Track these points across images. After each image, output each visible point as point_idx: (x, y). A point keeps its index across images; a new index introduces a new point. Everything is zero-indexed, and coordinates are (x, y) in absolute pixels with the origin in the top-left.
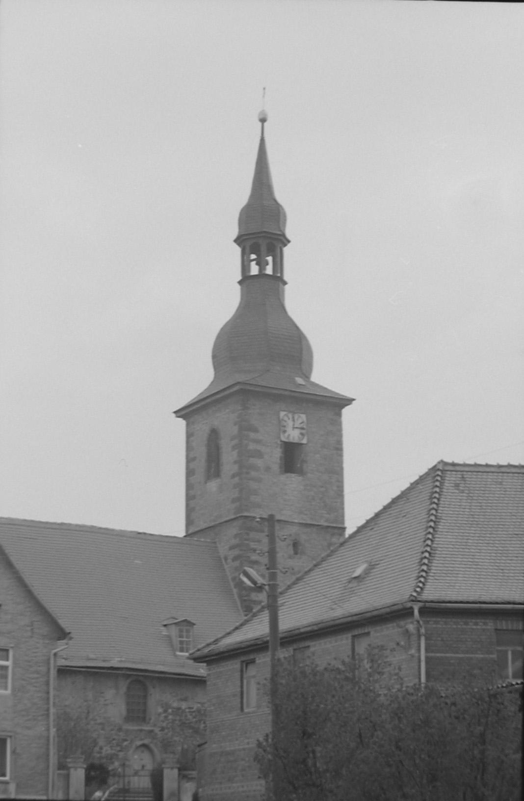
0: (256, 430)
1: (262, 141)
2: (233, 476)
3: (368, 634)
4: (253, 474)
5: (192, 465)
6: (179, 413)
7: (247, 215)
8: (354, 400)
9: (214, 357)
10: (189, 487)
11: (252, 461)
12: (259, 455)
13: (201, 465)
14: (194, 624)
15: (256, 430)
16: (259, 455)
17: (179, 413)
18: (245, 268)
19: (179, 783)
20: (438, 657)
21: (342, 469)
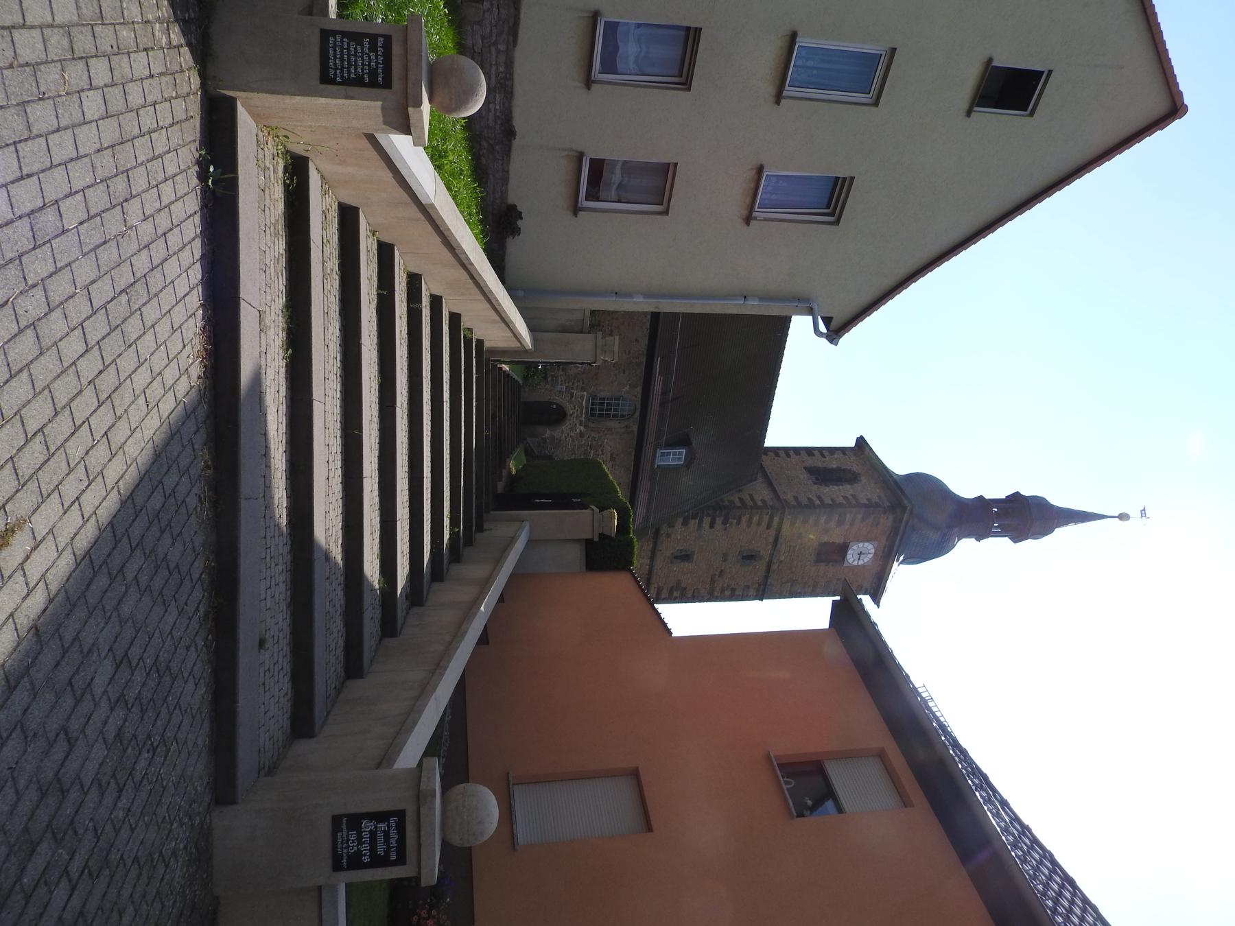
2: (819, 498)
3: (906, 803)
5: (803, 453)
6: (861, 441)
10: (797, 450)
11: (836, 517)
12: (840, 523)
13: (818, 462)
16: (840, 523)
17: (861, 441)
19: (419, 873)
20: (793, 804)
21: (816, 596)
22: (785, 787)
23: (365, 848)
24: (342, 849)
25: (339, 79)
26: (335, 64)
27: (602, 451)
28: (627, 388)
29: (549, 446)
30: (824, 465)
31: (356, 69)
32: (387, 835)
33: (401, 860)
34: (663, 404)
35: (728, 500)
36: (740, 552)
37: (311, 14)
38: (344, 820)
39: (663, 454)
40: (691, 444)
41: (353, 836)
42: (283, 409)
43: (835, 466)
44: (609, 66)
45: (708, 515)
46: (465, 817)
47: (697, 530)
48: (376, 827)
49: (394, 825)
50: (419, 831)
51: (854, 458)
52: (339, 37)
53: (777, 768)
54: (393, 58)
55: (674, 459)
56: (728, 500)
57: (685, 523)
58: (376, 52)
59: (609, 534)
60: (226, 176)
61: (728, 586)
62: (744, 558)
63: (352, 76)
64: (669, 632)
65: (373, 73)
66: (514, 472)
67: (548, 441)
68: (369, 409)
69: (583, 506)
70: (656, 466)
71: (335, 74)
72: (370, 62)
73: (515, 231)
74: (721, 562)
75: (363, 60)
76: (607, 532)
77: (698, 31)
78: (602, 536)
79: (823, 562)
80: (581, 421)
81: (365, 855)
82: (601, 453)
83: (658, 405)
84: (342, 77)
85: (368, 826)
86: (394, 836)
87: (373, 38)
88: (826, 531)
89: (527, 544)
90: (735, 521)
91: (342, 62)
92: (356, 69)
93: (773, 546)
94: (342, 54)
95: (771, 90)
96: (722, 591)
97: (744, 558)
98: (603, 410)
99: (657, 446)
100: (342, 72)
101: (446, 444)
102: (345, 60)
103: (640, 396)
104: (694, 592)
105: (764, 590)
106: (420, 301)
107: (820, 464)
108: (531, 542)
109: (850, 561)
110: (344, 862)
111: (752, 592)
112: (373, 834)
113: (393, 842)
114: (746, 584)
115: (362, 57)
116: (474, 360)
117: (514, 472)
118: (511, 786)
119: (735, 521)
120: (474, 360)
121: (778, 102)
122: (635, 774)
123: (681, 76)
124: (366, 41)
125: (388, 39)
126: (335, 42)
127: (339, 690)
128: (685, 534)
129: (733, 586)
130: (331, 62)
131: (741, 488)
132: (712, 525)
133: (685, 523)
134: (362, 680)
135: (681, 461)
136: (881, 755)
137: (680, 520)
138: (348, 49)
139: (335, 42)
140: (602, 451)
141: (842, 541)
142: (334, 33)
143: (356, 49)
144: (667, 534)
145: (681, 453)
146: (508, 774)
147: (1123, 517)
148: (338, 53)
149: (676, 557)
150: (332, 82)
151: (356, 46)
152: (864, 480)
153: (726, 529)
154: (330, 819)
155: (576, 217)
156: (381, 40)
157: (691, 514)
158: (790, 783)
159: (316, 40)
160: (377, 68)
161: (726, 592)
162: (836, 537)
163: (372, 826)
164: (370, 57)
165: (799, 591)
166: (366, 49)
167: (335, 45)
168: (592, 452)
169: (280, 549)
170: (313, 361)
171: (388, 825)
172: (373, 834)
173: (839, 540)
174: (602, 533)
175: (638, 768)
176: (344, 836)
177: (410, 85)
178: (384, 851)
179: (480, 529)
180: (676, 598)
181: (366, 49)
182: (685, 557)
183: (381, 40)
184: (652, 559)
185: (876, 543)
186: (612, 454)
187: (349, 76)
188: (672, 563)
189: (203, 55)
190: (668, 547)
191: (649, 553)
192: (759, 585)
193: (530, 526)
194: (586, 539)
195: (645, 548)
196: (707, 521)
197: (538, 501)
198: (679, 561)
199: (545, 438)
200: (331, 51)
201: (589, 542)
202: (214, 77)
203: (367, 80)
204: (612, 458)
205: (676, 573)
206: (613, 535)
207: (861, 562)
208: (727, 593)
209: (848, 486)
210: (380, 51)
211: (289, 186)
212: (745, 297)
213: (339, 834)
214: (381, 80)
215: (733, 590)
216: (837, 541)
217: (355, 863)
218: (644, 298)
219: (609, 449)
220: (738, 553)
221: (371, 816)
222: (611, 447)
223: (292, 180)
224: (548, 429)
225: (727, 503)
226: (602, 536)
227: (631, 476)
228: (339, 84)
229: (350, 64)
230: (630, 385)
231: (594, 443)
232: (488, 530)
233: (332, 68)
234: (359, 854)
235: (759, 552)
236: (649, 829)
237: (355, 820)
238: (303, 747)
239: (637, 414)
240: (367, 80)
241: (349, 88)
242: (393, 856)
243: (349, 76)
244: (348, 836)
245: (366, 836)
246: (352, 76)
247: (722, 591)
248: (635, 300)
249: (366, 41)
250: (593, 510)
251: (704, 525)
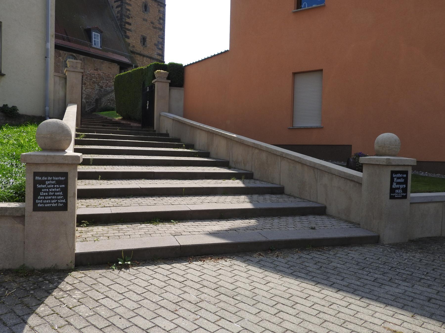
19: (411, 165)
22: (307, 8)
23: (401, 186)
24: (400, 195)
25: (64, 201)
26: (55, 203)
27: (93, 74)
28: (61, 58)
29: (90, 100)
31: (57, 192)
32: (398, 178)
33: (406, 173)
34: (69, 41)
35: (117, 14)
36: (143, 12)
37: (23, 216)
38: (392, 194)
39: (95, 44)
40: (90, 28)
41: (397, 191)
42: (214, 223)
45: (125, 25)
46: (393, 147)
47: (132, 32)
48: (395, 182)
49: (395, 175)
50: (398, 165)
52: (37, 201)
53: (299, 10)
54: (48, 171)
55: (98, 39)
56: (117, 14)
57: (128, 37)
58: (45, 181)
59: (167, 75)
60: (123, 257)
61: (158, 20)
62: (146, 10)
63: (61, 193)
64: (226, 52)
65: (59, 182)
66: (120, 118)
67: (87, 101)
68: (130, 185)
69: (152, 87)
70: (101, 48)
71: (61, 203)
72: (52, 184)
73: (14, 109)
74: (147, 22)
75: (51, 188)
76: (166, 76)
78: (168, 78)
81: (403, 186)
82: (93, 75)
83: (63, 41)
84: (62, 199)
85: (394, 186)
87: (36, 182)
89: (170, 113)
90: (128, 12)
91: (54, 199)
92: (57, 192)
94: (48, 199)
96: (160, 24)
97: (146, 10)
99: (91, 46)
100: (59, 199)
101: (131, 148)
102: (52, 198)
103: (65, 52)
104: (160, 38)
105: (161, 3)
106: (89, 159)
108: (170, 112)
110: (404, 194)
111: (162, 9)
112: (398, 183)
113: (401, 176)
114: (158, 12)
115: (49, 188)
116: (89, 134)
117: (120, 118)
118: (293, 128)
119: (128, 12)
120: (89, 134)
122: (295, 74)
125: (36, 174)
126: (41, 203)
127: (290, 196)
128: (133, 38)
129: (158, 18)
130: (53, 205)
131: (111, 6)
132: (130, 24)
133: (128, 37)
134: (285, 188)
135: (98, 35)
137: (127, 40)
138: (45, 196)
139: (41, 203)
140: (93, 74)
142: (35, 204)
143: (44, 192)
144: (133, 47)
145: (95, 35)
146: (289, 129)
148: (48, 201)
149: (144, 44)
151: (43, 192)
153: (132, 17)
154: (390, 200)
155: (5, 75)
156: (37, 178)
157: (124, 34)
158: (305, 4)
159: (39, 214)
160: (56, 180)
161: (161, 22)
163: (395, 184)
164: (49, 184)
166: (44, 186)
167: (43, 203)
168: (93, 79)
169: (268, 222)
170: (173, 210)
171: (395, 177)
172: (398, 183)
176: (396, 194)
177: (66, 162)
178: (45, 177)
179: (167, 135)
180: (162, 47)
181: (44, 186)
182: (144, 40)
183: (37, 178)
184: (144, 56)
186: (95, 70)
187: (62, 195)
188: (146, 47)
189: (66, 272)
190: (139, 48)
191: (141, 57)
192: (159, 5)
193: (162, 112)
194: (169, 86)
195: (139, 59)
196: (127, 26)
197: (148, 107)
198: (145, 43)
199: (86, 102)
200: (46, 205)
201: (171, 85)
202: (67, 265)
203: (63, 186)
204: (97, 70)
205: (151, 45)
206: (168, 73)
208: (161, 21)
210: (44, 178)
211: (87, 224)
213: (396, 196)
214: (62, 178)
215: (160, 18)
217: (405, 190)
218: (48, 42)
219: (92, 71)
220: (143, 13)
222: (91, 70)
223: (84, 223)
225: (119, 15)
226: (168, 78)
227: (105, 61)
228: (66, 200)
229: (54, 195)
230: (59, 56)
231: (89, 78)
232: (167, 131)
233: (57, 205)
235: (143, 2)
236: (321, 70)
237: (392, 190)
238: (332, 209)
239: (74, 54)
240: (63, 186)
241: (69, 195)
242: (405, 176)
243: (62, 195)
244: (397, 193)
245: (398, 186)
246: (61, 193)
247: (160, 24)
248: (49, 48)
250: (156, 82)
251: (130, 28)
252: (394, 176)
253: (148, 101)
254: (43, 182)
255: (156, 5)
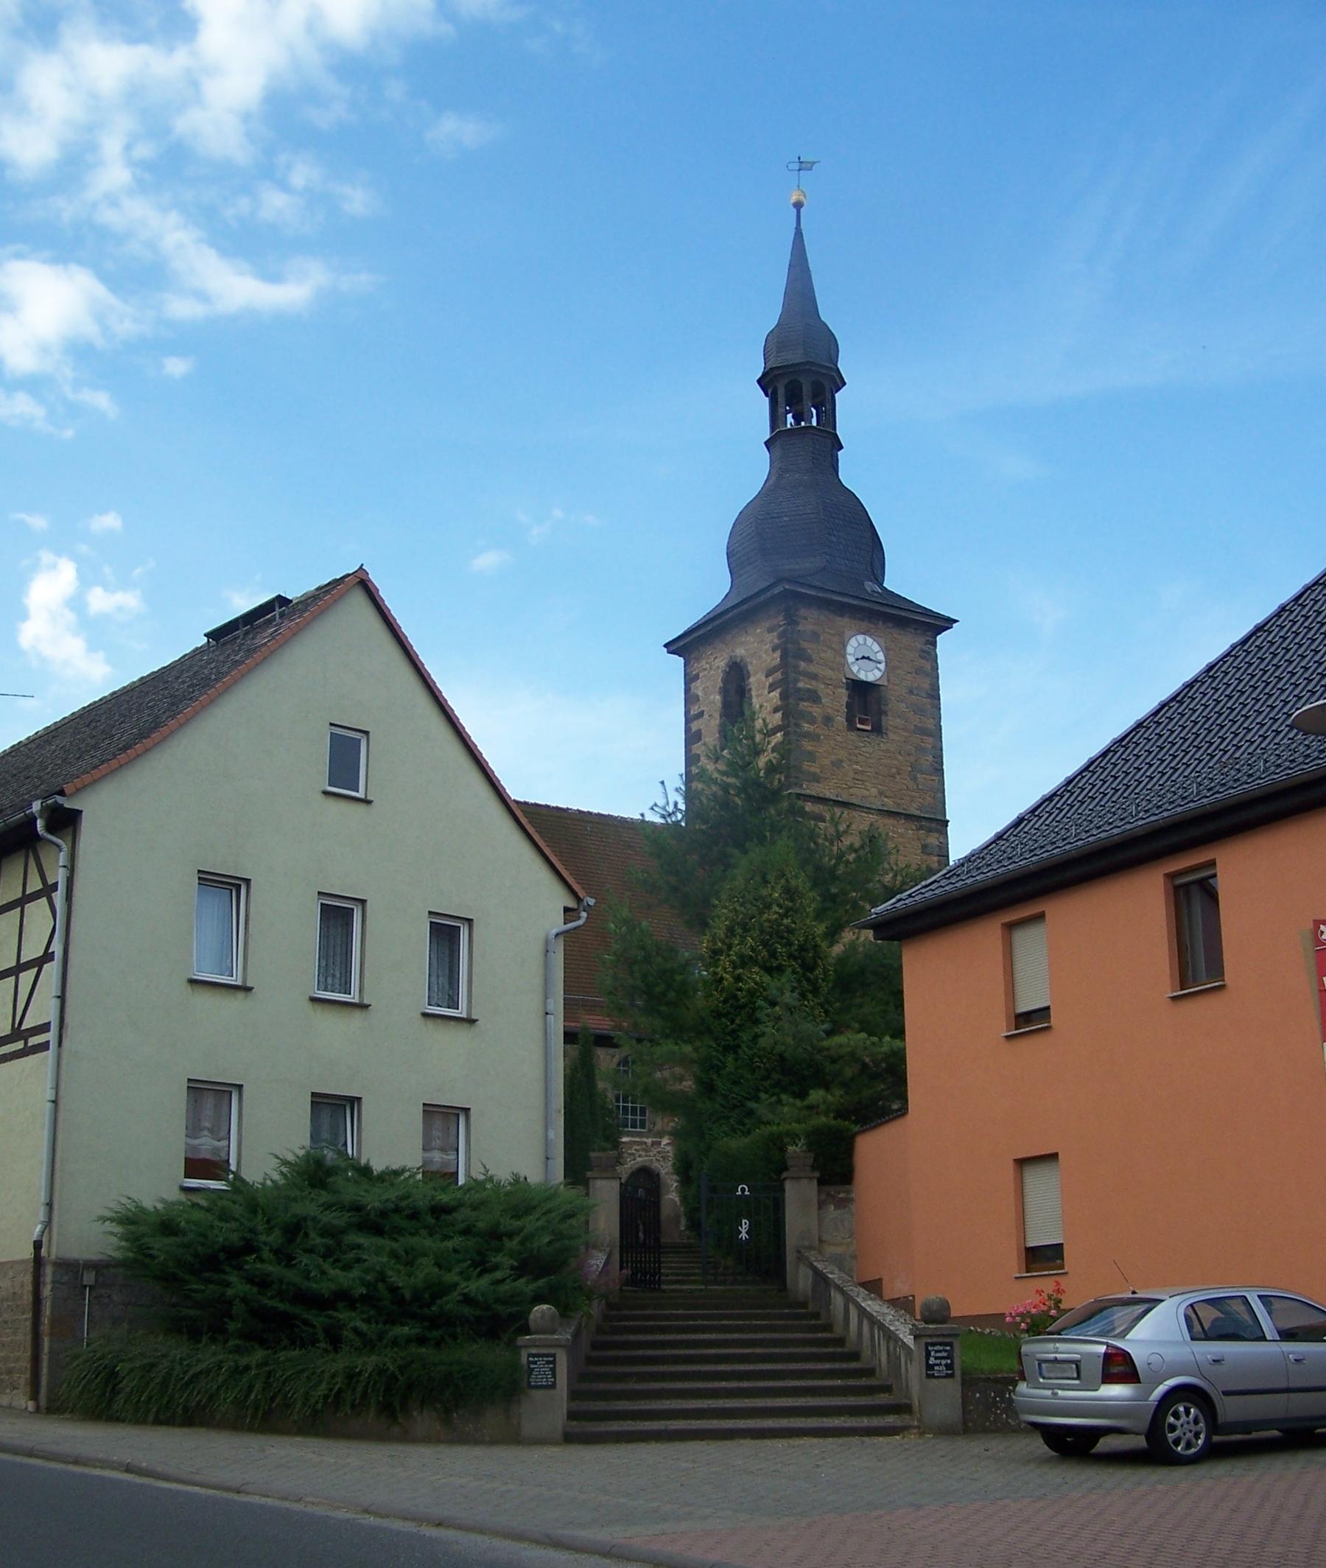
0: (809, 660)
1: (799, 234)
3: (1040, 917)
4: (806, 727)
5: (695, 727)
6: (673, 647)
7: (776, 342)
8: (956, 621)
9: (730, 555)
11: (804, 705)
14: (477, 1020)
15: (809, 660)
16: (814, 697)
18: (775, 419)
23: (944, 1362)
30: (717, 715)
32: (936, 1352)
41: (936, 1368)
43: (718, 697)
44: (816, 1316)
51: (703, 663)
52: (531, 1380)
65: (548, 1362)
77: (312, 1093)
79: (881, 720)
80: (653, 1144)
85: (932, 1361)
86: (938, 1348)
88: (828, 720)
93: (855, 810)
95: (358, 1014)
98: (634, 1109)
107: (716, 721)
109: (878, 674)
110: (949, 1372)
113: (941, 1348)
114: (919, 851)
121: (367, 1006)
122: (1022, 1163)
123: (345, 1106)
124: (532, 1366)
136: (1011, 927)
141: (844, 691)
147: (798, 205)
150: (554, 1383)
152: (740, 652)
156: (531, 1359)
162: (836, 701)
165: (930, 758)
173: (843, 694)
174: (812, 1167)
175: (1015, 1160)
183: (531, 1359)
185: (848, 633)
192: (921, 828)
207: (881, 656)
209: (752, 679)
210: (536, 1359)
212: (547, 1013)
216: (845, 699)
221: (927, 1359)
224: (667, 1197)
234: (946, 1365)
236: (1053, 1157)
242: (948, 1348)
245: (938, 1362)
249: (532, 1366)
252: (930, 1348)
253: (744, 1235)
254: (535, 1363)
255: (910, 832)
